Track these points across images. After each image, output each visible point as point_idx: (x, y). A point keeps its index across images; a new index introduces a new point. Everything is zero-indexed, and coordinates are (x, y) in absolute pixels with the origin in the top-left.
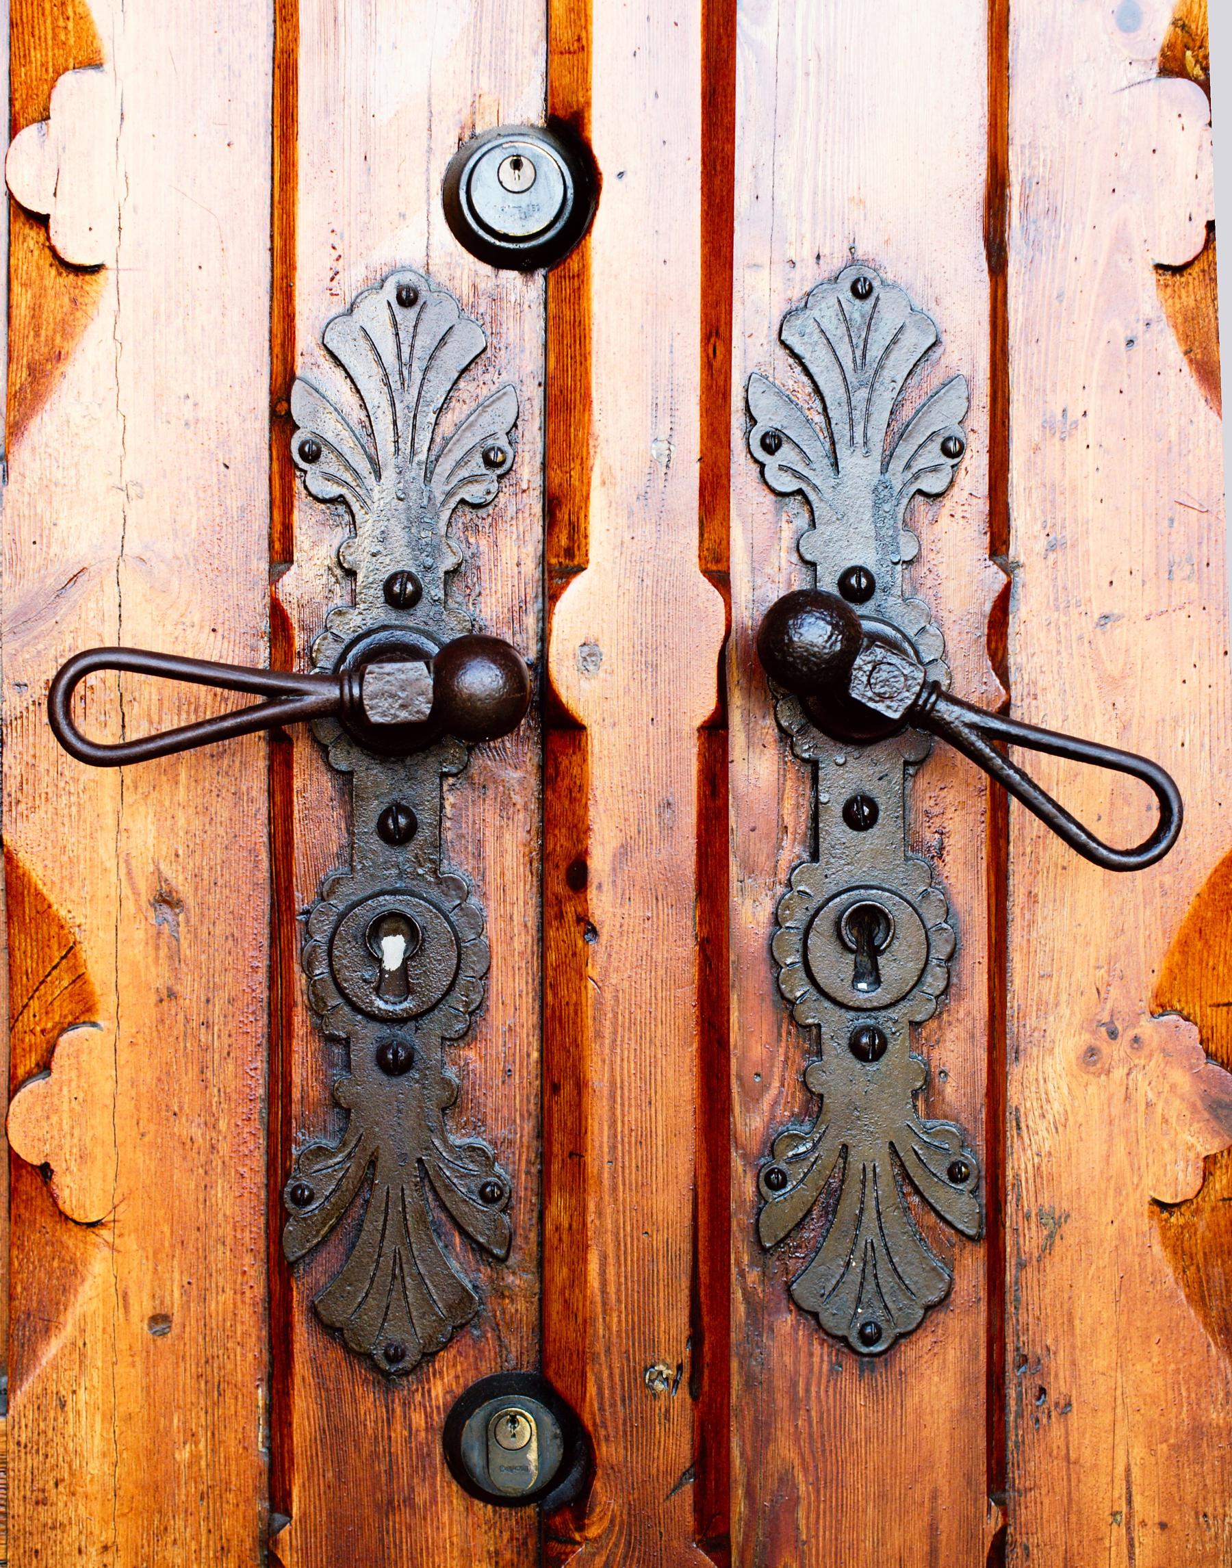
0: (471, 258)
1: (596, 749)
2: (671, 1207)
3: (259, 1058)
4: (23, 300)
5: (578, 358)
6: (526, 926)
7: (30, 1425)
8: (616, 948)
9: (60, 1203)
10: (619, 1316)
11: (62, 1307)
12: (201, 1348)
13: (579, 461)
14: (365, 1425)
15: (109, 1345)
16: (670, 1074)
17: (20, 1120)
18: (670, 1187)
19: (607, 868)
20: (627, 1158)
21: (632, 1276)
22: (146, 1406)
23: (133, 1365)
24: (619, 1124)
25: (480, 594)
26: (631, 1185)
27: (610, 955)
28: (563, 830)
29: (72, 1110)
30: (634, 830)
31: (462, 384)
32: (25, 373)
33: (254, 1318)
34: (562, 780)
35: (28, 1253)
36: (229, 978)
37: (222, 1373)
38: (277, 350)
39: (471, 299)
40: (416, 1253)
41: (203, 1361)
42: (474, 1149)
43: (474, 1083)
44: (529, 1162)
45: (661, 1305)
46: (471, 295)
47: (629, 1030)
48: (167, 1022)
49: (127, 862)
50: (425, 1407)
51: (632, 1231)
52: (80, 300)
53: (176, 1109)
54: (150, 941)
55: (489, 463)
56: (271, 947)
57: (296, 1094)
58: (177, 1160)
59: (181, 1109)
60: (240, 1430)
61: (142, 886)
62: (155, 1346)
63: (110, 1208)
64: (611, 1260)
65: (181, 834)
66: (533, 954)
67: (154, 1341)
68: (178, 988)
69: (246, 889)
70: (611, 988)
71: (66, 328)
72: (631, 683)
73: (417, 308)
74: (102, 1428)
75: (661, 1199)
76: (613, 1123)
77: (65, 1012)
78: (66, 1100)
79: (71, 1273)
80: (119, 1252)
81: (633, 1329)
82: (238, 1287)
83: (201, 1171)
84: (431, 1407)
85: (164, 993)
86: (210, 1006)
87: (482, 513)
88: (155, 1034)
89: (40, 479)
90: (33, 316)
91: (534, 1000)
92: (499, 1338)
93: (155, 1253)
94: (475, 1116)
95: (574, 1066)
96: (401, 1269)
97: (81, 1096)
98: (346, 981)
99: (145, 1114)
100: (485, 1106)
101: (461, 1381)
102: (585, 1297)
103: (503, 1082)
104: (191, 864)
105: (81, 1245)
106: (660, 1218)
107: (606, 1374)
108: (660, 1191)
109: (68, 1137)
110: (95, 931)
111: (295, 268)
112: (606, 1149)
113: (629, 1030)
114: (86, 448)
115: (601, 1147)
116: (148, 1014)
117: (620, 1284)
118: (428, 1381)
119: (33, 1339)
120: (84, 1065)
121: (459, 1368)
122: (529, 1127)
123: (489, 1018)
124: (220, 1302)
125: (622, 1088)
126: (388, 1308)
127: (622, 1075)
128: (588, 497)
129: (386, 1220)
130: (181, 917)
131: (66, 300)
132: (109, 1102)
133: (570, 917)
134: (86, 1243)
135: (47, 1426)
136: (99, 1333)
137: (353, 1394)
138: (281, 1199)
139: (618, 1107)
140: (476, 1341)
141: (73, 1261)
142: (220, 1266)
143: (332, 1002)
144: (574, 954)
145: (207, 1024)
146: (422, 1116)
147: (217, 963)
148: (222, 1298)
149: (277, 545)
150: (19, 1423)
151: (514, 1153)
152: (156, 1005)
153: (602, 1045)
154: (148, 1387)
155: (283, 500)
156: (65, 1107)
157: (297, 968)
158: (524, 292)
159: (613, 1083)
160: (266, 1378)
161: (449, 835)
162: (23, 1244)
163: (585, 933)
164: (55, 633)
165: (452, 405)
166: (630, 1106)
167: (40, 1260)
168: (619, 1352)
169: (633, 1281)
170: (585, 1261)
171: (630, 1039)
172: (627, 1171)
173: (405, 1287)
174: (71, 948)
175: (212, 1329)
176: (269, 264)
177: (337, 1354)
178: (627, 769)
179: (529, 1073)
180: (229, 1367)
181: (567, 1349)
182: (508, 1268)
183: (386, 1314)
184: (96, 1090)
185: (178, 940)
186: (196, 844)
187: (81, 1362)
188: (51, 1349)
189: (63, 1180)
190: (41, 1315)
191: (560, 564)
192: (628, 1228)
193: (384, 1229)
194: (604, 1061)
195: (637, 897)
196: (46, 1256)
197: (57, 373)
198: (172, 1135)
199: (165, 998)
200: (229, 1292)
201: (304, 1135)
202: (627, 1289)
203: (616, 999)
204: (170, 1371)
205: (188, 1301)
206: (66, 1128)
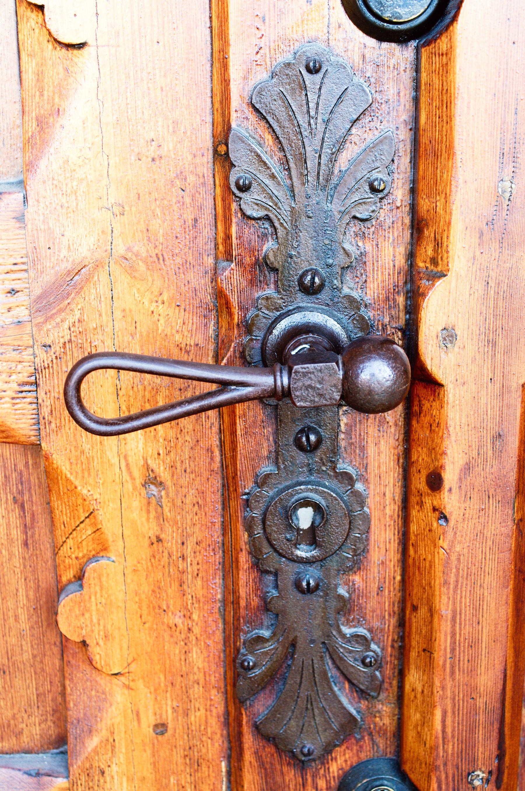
0: (360, 33)
1: (451, 400)
2: (489, 683)
3: (217, 577)
4: (30, 67)
5: (445, 118)
6: (394, 500)
7: (83, 783)
8: (460, 528)
9: (94, 663)
10: (453, 745)
11: (99, 719)
12: (186, 741)
13: (444, 195)
14: (289, 788)
15: (129, 741)
16: (493, 605)
17: (65, 616)
18: (489, 671)
19: (456, 478)
20: (462, 655)
21: (462, 723)
22: (154, 773)
23: (145, 751)
24: (458, 636)
25: (366, 281)
26: (464, 671)
27: (455, 533)
28: (425, 449)
29: (98, 610)
30: (475, 453)
31: (354, 131)
32: (34, 125)
33: (219, 724)
34: (425, 416)
35: (76, 684)
36: (197, 529)
37: (200, 754)
38: (217, 105)
39: (361, 66)
40: (321, 696)
41: (187, 748)
42: (358, 636)
43: (359, 596)
44: (393, 640)
45: (480, 738)
46: (361, 62)
47: (467, 579)
48: (157, 557)
49: (125, 457)
50: (326, 777)
51: (463, 697)
52: (71, 69)
53: (165, 608)
54: (144, 508)
55: (374, 190)
56: (223, 509)
57: (243, 603)
58: (167, 637)
59: (168, 607)
60: (212, 784)
61: (136, 474)
62: (158, 740)
63: (126, 665)
64: (449, 714)
65: (161, 440)
66: (398, 516)
67: (157, 738)
68: (163, 536)
69: (206, 474)
70: (456, 554)
71: (61, 90)
72: (477, 354)
73: (320, 75)
74: (127, 785)
75: (482, 678)
76: (453, 635)
77: (90, 548)
78: (94, 604)
79: (104, 698)
80: (132, 689)
81: (462, 752)
82: (208, 707)
83: (182, 643)
84: (330, 776)
85: (154, 540)
86: (185, 547)
87: (368, 224)
88: (149, 564)
89: (51, 203)
90: (38, 80)
91: (399, 544)
92: (372, 739)
93: (155, 690)
94: (358, 615)
95: (428, 599)
96: (312, 704)
97: (104, 601)
98: (275, 540)
99: (145, 612)
100: (366, 609)
101: (349, 763)
102: (431, 734)
103: (378, 594)
104: (169, 459)
105: (109, 685)
106: (482, 689)
107: (443, 776)
108: (483, 674)
109: (97, 626)
110: (107, 502)
111: (229, 45)
112: (448, 650)
113: (467, 579)
114: (82, 180)
115: (445, 649)
116: (145, 552)
117: (454, 727)
118: (328, 763)
119: (82, 735)
120: (104, 583)
121: (347, 756)
122: (393, 621)
123: (369, 557)
124: (197, 717)
125: (460, 614)
126: (303, 725)
127: (461, 606)
128: (450, 223)
129: (301, 678)
130: (163, 493)
131: (61, 69)
132: (122, 605)
133: (428, 505)
134: (111, 683)
135: (94, 784)
136: (123, 735)
137: (281, 771)
138: (235, 669)
139: (458, 625)
140: (358, 741)
141: (104, 693)
142: (196, 696)
143: (265, 550)
144: (430, 530)
145: (183, 558)
146: (325, 618)
147: (188, 521)
148: (198, 714)
149: (221, 247)
150: (77, 783)
151: (384, 636)
152: (149, 546)
153: (448, 588)
154: (154, 763)
155: (225, 217)
156: (94, 608)
157: (240, 527)
158: (402, 55)
159: (454, 612)
160: (226, 756)
161: (343, 444)
162: (72, 679)
163: (439, 519)
164: (67, 311)
165: (346, 146)
166: (465, 625)
167: (83, 689)
168: (453, 765)
169: (463, 725)
170: (432, 714)
171: (467, 584)
172: (462, 663)
173: (314, 714)
174: (92, 513)
175: (192, 731)
176: (209, 39)
177: (270, 749)
178: (472, 413)
179: (394, 589)
180: (204, 750)
181: (418, 759)
182: (379, 701)
183: (302, 729)
184: (113, 598)
185: (161, 507)
186: (171, 447)
187: (112, 750)
188: (93, 743)
189: (95, 650)
190: (86, 722)
191: (427, 268)
192: (461, 696)
193: (301, 683)
194: (449, 598)
195: (475, 496)
196: (87, 688)
197: (58, 125)
198: (163, 623)
199: (155, 542)
200: (203, 711)
201: (248, 627)
202: (458, 730)
203: (459, 560)
204: (168, 754)
205: (177, 716)
206: (95, 620)
